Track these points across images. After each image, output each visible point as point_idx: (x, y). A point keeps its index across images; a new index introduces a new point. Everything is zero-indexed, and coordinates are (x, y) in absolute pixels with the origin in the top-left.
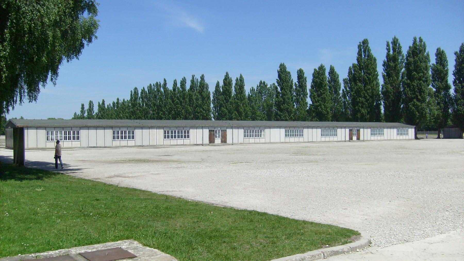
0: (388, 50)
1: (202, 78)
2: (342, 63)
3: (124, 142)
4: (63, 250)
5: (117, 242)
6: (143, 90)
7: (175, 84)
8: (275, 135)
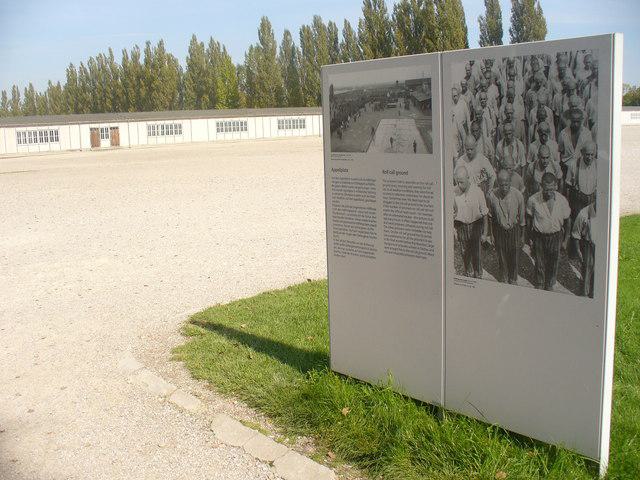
7: (125, 59)
8: (200, 129)
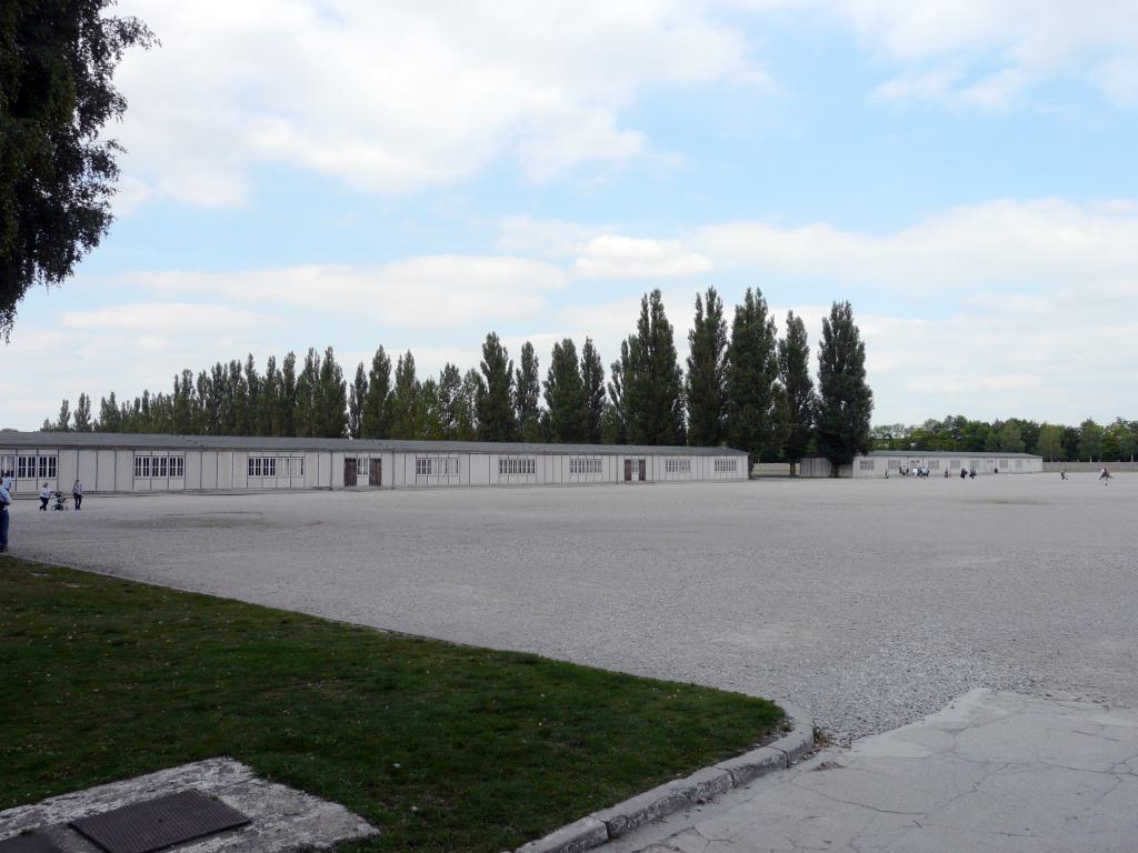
1: (329, 354)
4: (18, 809)
5: (183, 770)
6: (202, 378)
7: (272, 364)
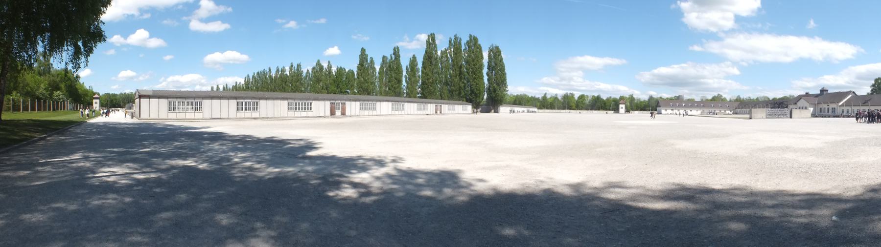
0: (112, 102)
2: (242, 81)
3: (248, 114)
6: (253, 76)
7: (278, 70)
